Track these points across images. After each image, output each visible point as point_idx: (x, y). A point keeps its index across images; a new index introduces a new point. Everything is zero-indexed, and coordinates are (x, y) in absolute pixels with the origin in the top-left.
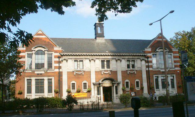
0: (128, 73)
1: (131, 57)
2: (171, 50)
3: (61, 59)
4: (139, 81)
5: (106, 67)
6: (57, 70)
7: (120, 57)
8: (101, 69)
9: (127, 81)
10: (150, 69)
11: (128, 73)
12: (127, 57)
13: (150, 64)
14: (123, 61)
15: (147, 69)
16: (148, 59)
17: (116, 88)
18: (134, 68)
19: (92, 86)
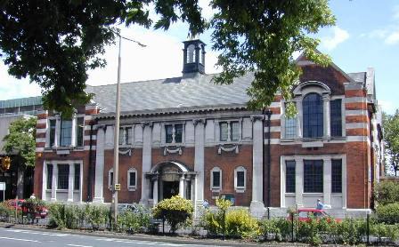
0: (219, 151)
1: (229, 114)
2: (341, 87)
3: (95, 127)
4: (245, 171)
5: (174, 141)
6: (87, 148)
7: (203, 115)
8: (164, 144)
9: (216, 169)
10: (274, 141)
11: (219, 151)
12: (218, 115)
13: (273, 129)
14: (210, 123)
15: (266, 142)
16: (269, 117)
17: (287, 177)
18: (181, 141)
19: (144, 181)
